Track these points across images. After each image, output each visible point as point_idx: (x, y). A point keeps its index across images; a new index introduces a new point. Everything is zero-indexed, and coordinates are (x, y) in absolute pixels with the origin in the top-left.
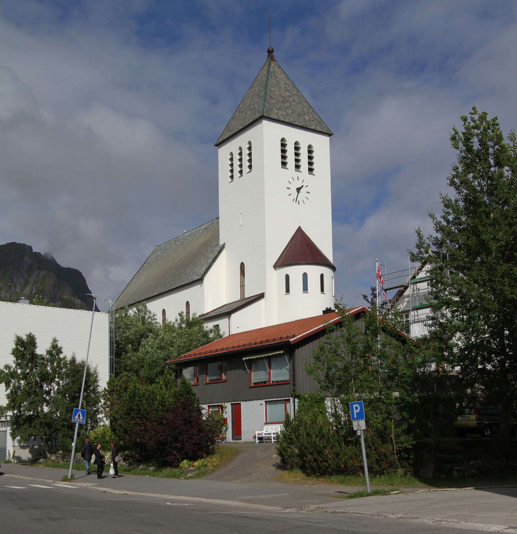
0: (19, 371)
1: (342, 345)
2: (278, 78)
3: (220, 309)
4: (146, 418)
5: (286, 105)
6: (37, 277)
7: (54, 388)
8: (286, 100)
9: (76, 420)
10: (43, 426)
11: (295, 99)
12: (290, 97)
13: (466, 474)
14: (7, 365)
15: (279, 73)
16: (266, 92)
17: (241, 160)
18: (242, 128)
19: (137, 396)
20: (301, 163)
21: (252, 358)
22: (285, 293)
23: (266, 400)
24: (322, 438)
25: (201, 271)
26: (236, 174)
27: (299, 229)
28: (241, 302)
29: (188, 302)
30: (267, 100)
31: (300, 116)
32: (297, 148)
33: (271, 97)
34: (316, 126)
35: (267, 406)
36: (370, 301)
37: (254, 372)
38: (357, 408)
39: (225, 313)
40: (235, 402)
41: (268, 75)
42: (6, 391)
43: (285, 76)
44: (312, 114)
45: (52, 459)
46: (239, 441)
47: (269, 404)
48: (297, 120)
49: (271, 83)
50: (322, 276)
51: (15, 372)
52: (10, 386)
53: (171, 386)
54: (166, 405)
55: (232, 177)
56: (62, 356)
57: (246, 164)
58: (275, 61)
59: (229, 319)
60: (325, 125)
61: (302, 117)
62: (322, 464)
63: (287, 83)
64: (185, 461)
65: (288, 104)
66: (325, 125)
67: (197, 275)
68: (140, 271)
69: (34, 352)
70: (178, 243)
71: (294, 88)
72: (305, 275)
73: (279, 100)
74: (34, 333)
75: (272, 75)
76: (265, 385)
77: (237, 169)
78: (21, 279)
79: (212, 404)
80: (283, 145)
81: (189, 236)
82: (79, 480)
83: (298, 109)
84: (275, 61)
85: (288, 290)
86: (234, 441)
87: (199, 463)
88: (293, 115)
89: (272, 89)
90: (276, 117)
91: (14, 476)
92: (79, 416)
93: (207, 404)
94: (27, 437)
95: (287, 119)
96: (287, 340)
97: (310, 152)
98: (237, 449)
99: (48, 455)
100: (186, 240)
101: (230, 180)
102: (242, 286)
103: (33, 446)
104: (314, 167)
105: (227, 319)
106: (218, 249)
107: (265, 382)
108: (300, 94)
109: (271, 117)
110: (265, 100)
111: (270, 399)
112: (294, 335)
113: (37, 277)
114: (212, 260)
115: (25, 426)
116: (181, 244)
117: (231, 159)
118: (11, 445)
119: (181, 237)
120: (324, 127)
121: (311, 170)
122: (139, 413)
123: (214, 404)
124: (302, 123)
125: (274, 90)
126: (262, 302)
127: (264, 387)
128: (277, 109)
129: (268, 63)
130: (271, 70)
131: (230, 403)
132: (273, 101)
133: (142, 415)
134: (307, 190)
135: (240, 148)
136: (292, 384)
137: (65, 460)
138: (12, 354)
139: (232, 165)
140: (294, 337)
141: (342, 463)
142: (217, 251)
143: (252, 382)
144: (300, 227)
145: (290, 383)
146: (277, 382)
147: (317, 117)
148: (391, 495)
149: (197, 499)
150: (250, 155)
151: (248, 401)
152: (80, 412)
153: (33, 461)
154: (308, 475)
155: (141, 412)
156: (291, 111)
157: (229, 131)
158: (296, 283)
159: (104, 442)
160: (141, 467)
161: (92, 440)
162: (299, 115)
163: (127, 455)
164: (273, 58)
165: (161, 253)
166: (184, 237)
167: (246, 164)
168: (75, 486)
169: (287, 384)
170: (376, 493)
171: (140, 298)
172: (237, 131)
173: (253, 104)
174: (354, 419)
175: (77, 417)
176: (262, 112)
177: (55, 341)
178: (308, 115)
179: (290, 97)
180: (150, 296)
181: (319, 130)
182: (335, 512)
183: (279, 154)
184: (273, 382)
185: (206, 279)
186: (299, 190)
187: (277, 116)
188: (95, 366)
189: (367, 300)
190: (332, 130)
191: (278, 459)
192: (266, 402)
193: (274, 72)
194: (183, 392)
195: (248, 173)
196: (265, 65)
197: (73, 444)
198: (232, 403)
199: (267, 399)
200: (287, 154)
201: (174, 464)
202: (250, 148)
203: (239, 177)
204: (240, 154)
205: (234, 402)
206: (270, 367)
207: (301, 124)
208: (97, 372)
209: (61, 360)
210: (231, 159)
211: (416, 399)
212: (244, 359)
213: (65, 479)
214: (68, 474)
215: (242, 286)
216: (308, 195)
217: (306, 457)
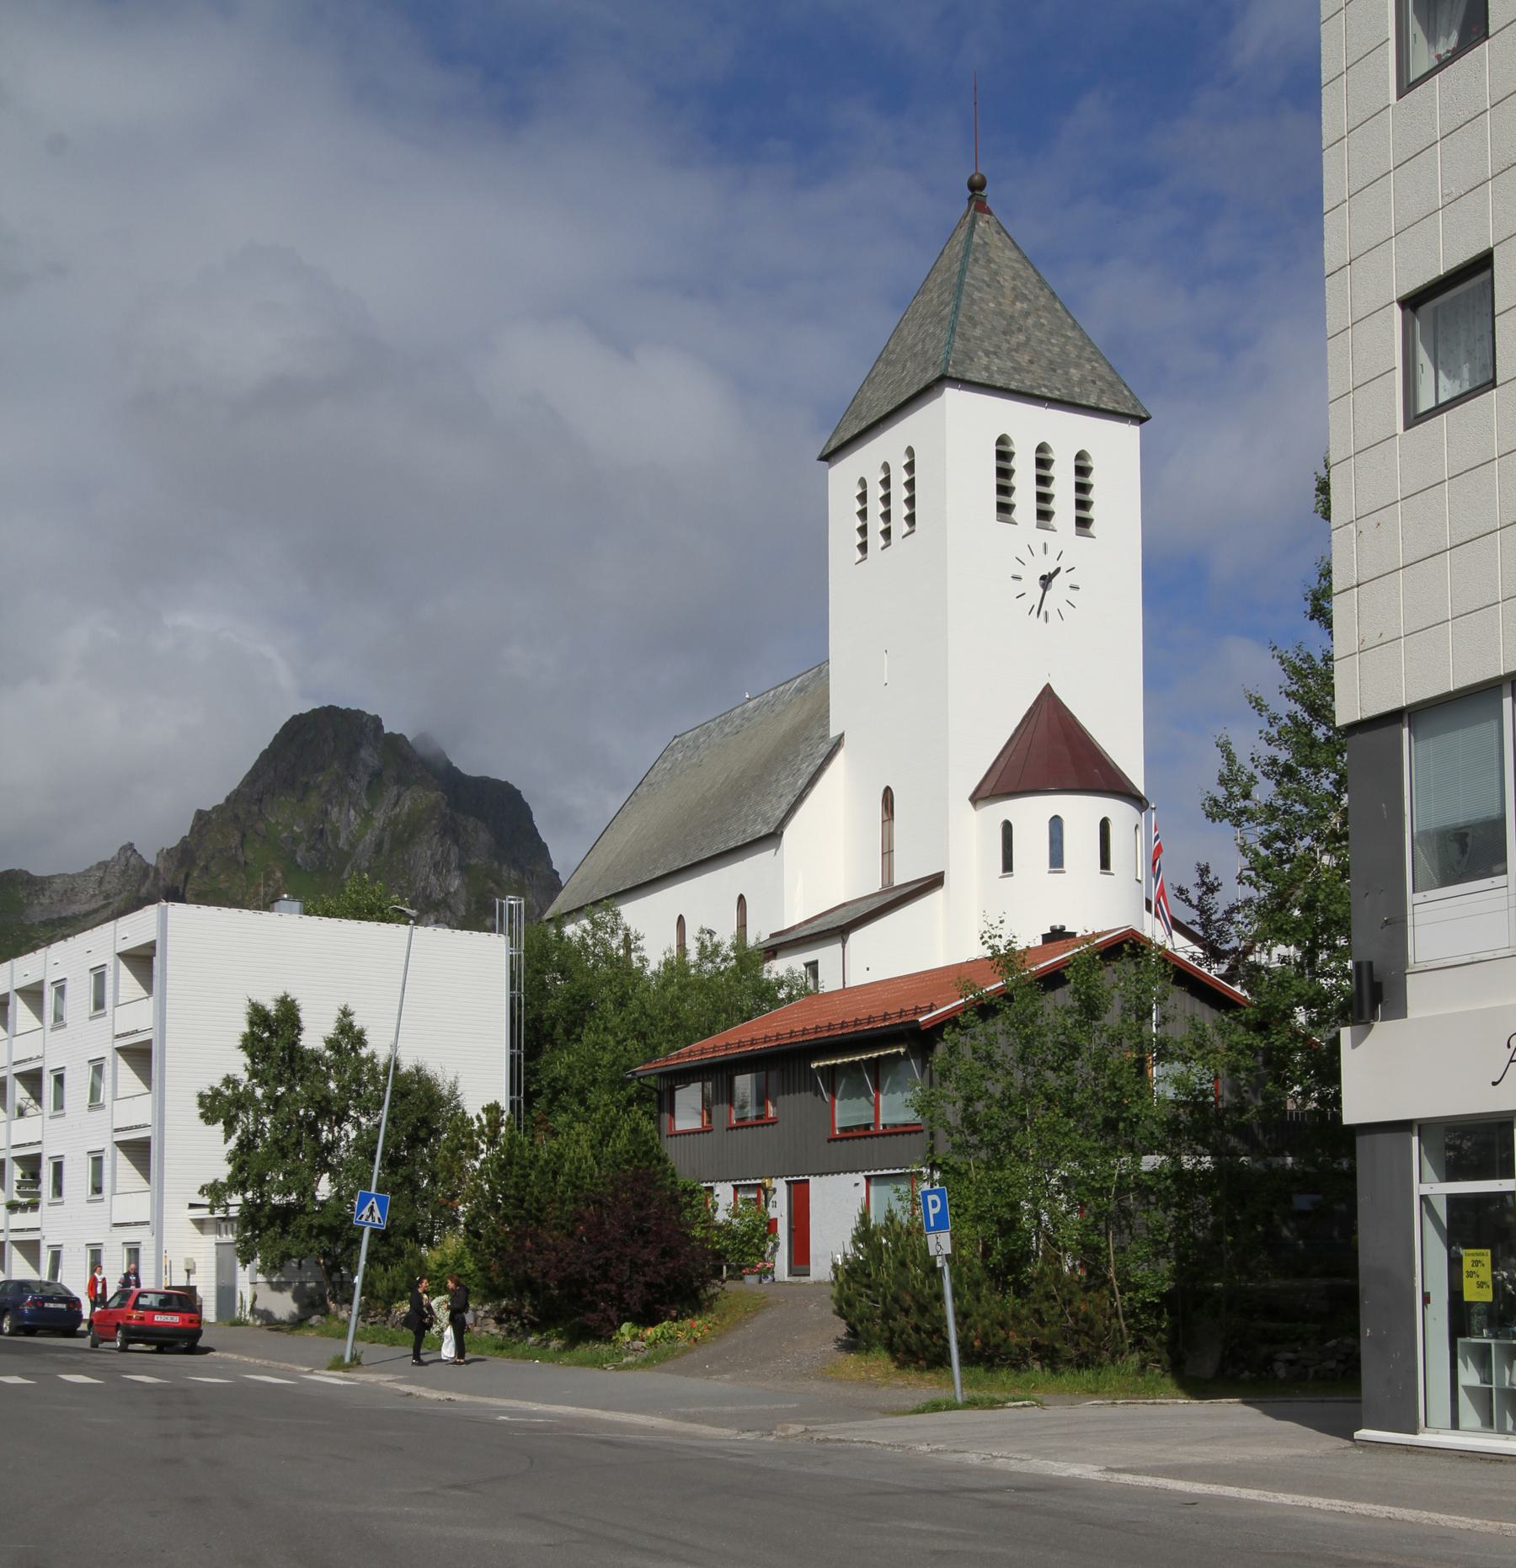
0: (259, 1092)
1: (1002, 1039)
2: (995, 262)
3: (828, 918)
4: (538, 1220)
5: (1014, 341)
6: (396, 804)
7: (347, 1135)
8: (1014, 327)
9: (363, 1220)
10: (314, 1233)
11: (1042, 320)
12: (1027, 314)
13: (1311, 1371)
14: (228, 1076)
15: (997, 247)
16: (957, 307)
17: (886, 499)
18: (890, 408)
19: (517, 1163)
20: (1054, 506)
21: (833, 1062)
22: (1001, 874)
23: (867, 1173)
24: (930, 1275)
25: (777, 812)
26: (875, 540)
27: (1048, 692)
28: (876, 899)
29: (741, 897)
30: (958, 330)
31: (1054, 370)
32: (1043, 463)
33: (971, 319)
34: (1099, 398)
35: (872, 1188)
36: (1195, 902)
37: (842, 1099)
38: (934, 1204)
39: (833, 929)
40: (795, 1178)
41: (966, 256)
42: (226, 1141)
43: (1014, 255)
44: (1089, 360)
45: (340, 1318)
46: (803, 1279)
47: (875, 1185)
48: (1046, 383)
49: (973, 278)
50: (1105, 825)
51: (249, 1095)
52: (234, 1131)
53: (618, 1136)
54: (585, 1186)
55: (863, 547)
56: (364, 1052)
57: (900, 510)
58: (990, 213)
59: (844, 947)
60: (1130, 391)
61: (1059, 371)
62: (931, 1339)
63: (1021, 277)
64: (626, 1327)
65: (1022, 338)
66: (1130, 391)
67: (766, 822)
68: (626, 809)
69: (295, 1043)
70: (727, 730)
71: (1042, 289)
72: (1056, 824)
73: (994, 328)
74: (293, 995)
75: (977, 254)
76: (867, 1133)
77: (876, 525)
78: (352, 812)
79: (879, 1172)
80: (1004, 455)
81: (755, 709)
82: (371, 1367)
83: (1049, 350)
84: (990, 213)
85: (1008, 866)
86: (792, 1279)
87: (656, 1332)
88: (1034, 367)
89: (977, 295)
90: (982, 377)
91: (230, 1356)
92: (372, 1209)
93: (730, 1181)
94: (277, 1261)
95: (1016, 380)
96: (914, 1018)
97: (1082, 471)
98: (764, 1298)
99: (332, 1305)
100: (749, 719)
101: (859, 556)
102: (888, 852)
103: (302, 1284)
104: (1093, 513)
105: (839, 945)
106: (824, 749)
107: (867, 1127)
108: (1058, 306)
109: (967, 378)
110: (953, 330)
111: (876, 1170)
112: (932, 1005)
113: (396, 804)
114: (806, 781)
115: (271, 1232)
116: (735, 731)
117: (863, 498)
118: (248, 1280)
119: (738, 711)
120: (1125, 397)
121: (1083, 523)
122: (521, 1207)
123: (748, 1182)
124: (1059, 390)
125: (982, 299)
126: (935, 898)
127: (875, 1139)
128: (987, 354)
129: (968, 218)
130: (976, 239)
131: (785, 1179)
132: (978, 332)
133: (529, 1211)
134: (1072, 578)
135: (886, 467)
136: (927, 1133)
137: (370, 1320)
138: (241, 1047)
139: (863, 514)
140: (931, 1011)
141: (977, 1338)
142: (822, 755)
143: (837, 1125)
144: (1048, 684)
145: (922, 1131)
146: (895, 1126)
147: (1103, 370)
148: (1006, 1410)
149: (1383, 1511)
150: (910, 485)
151: (827, 1174)
152: (374, 1200)
153: (297, 1323)
154: (902, 1365)
155: (525, 1205)
156: (1027, 358)
157: (856, 418)
158: (1032, 845)
159: (460, 1276)
160: (531, 1339)
161: (432, 1271)
162: (1052, 368)
163: (505, 1310)
164: (985, 204)
165: (684, 757)
166: (743, 712)
167: (900, 510)
168: (353, 1380)
169: (916, 1132)
170: (971, 1404)
171: (621, 885)
172: (876, 418)
173: (923, 341)
174: (930, 1229)
175: (366, 1212)
176: (943, 366)
177: (346, 1013)
178: (1078, 366)
179: (1027, 314)
180: (646, 879)
181: (1110, 406)
182: (828, 1440)
183: (992, 481)
184: (884, 1126)
185: (789, 833)
186: (1046, 580)
187: (985, 374)
188: (453, 1079)
189: (1187, 900)
190: (1151, 406)
191: (840, 1328)
192: (868, 1178)
193: (986, 244)
194: (631, 1153)
195: (904, 537)
196: (960, 225)
197: (357, 1278)
198: (790, 1179)
199: (869, 1171)
200: (1015, 481)
201: (602, 1332)
202: (910, 467)
203: (883, 549)
204: (886, 483)
205: (792, 1176)
206: (877, 1088)
207: (1056, 394)
208: (458, 1093)
209: (363, 1062)
210: (863, 498)
211: (1166, 1178)
212: (814, 1065)
213: (337, 1365)
214: (345, 1352)
215: (888, 852)
216: (1073, 595)
217: (895, 1319)
